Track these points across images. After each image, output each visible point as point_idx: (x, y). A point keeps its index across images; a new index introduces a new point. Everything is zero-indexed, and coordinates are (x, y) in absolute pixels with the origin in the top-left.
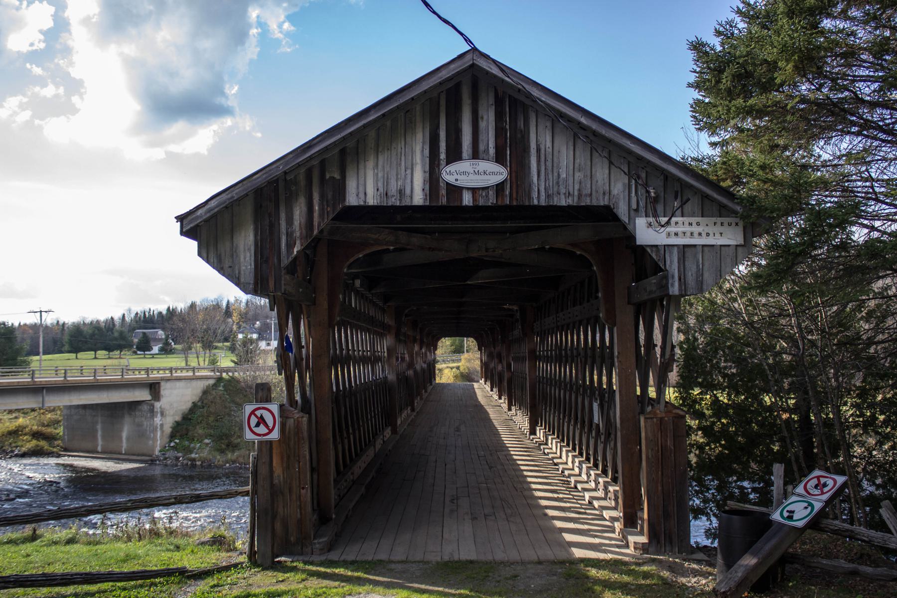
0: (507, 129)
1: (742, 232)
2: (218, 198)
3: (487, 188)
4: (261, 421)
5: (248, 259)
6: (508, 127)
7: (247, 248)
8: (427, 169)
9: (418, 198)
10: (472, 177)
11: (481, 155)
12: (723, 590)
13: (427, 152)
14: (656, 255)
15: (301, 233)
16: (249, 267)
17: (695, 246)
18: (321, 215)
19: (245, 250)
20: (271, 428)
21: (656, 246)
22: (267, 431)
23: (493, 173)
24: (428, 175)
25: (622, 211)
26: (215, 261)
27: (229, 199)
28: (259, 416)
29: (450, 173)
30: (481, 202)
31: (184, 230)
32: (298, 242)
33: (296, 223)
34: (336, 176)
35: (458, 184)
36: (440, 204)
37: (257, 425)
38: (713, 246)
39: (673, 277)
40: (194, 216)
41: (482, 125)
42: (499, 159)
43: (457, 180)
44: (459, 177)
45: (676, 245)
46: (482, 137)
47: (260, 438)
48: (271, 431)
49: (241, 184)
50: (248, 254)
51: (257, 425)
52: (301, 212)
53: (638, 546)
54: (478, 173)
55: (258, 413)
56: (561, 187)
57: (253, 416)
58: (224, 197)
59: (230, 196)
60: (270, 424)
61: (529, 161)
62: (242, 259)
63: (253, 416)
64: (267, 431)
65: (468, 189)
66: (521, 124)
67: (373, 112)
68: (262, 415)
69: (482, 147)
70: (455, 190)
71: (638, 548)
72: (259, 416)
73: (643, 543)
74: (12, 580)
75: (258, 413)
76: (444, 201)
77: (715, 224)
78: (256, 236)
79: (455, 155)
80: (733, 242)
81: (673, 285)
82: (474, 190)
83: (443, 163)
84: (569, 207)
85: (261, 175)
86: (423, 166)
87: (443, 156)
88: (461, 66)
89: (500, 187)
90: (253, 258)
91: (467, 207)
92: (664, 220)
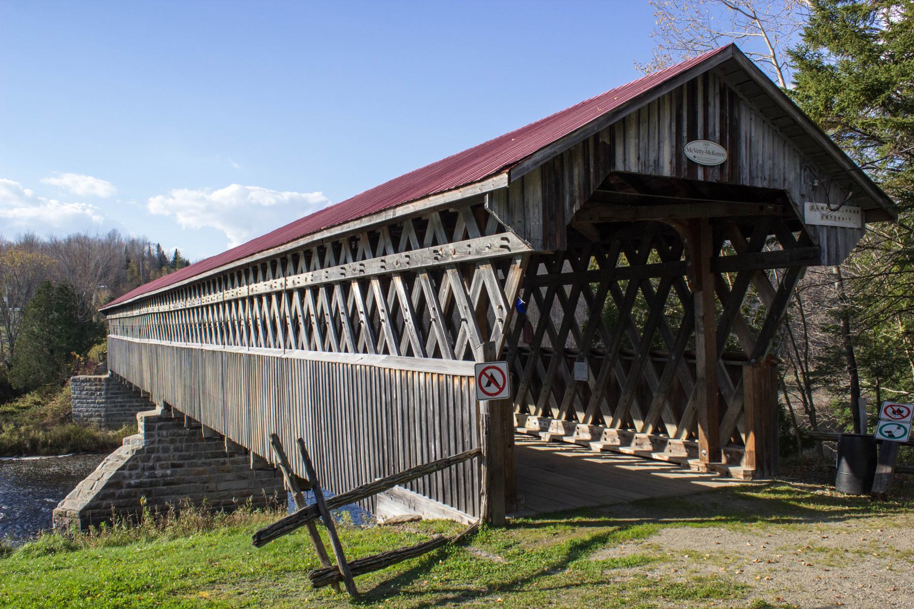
0: (726, 117)
1: (860, 219)
2: (542, 151)
3: (714, 166)
4: (491, 380)
5: (536, 215)
6: (728, 115)
7: (535, 204)
8: (674, 144)
9: (667, 171)
10: (705, 156)
11: (711, 137)
12: (881, 492)
13: (674, 128)
14: (814, 233)
15: (580, 193)
16: (538, 223)
17: (836, 227)
18: (597, 177)
19: (533, 205)
20: (501, 387)
21: (814, 226)
22: (498, 390)
23: (718, 154)
24: (674, 149)
25: (795, 196)
26: (505, 215)
27: (552, 154)
28: (489, 375)
29: (690, 150)
30: (710, 179)
31: (512, 181)
32: (578, 202)
33: (576, 183)
34: (606, 141)
35: (696, 160)
36: (683, 177)
37: (488, 385)
38: (845, 228)
39: (824, 251)
40: (521, 167)
41: (711, 110)
42: (722, 143)
43: (695, 157)
44: (696, 154)
45: (827, 226)
46: (711, 121)
47: (491, 397)
48: (501, 390)
49: (562, 140)
50: (536, 211)
51: (488, 385)
52: (579, 172)
53: (748, 474)
54: (708, 153)
55: (488, 372)
56: (759, 172)
57: (483, 376)
58: (548, 151)
59: (553, 150)
60: (501, 382)
61: (740, 147)
62: (531, 215)
63: (483, 376)
64: (498, 390)
65: (701, 165)
66: (736, 114)
67: (665, 87)
68: (492, 375)
69: (710, 130)
70: (692, 165)
71: (748, 475)
72: (489, 375)
73: (752, 471)
74: (358, 566)
75: (488, 372)
76: (684, 174)
77: (847, 211)
78: (543, 192)
79: (692, 137)
80: (856, 226)
81: (824, 258)
82: (705, 167)
83: (685, 140)
84: (763, 189)
85: (579, 134)
86: (671, 140)
87: (685, 134)
88: (724, 58)
89: (722, 166)
90: (541, 215)
91: (700, 182)
92: (833, 206)
